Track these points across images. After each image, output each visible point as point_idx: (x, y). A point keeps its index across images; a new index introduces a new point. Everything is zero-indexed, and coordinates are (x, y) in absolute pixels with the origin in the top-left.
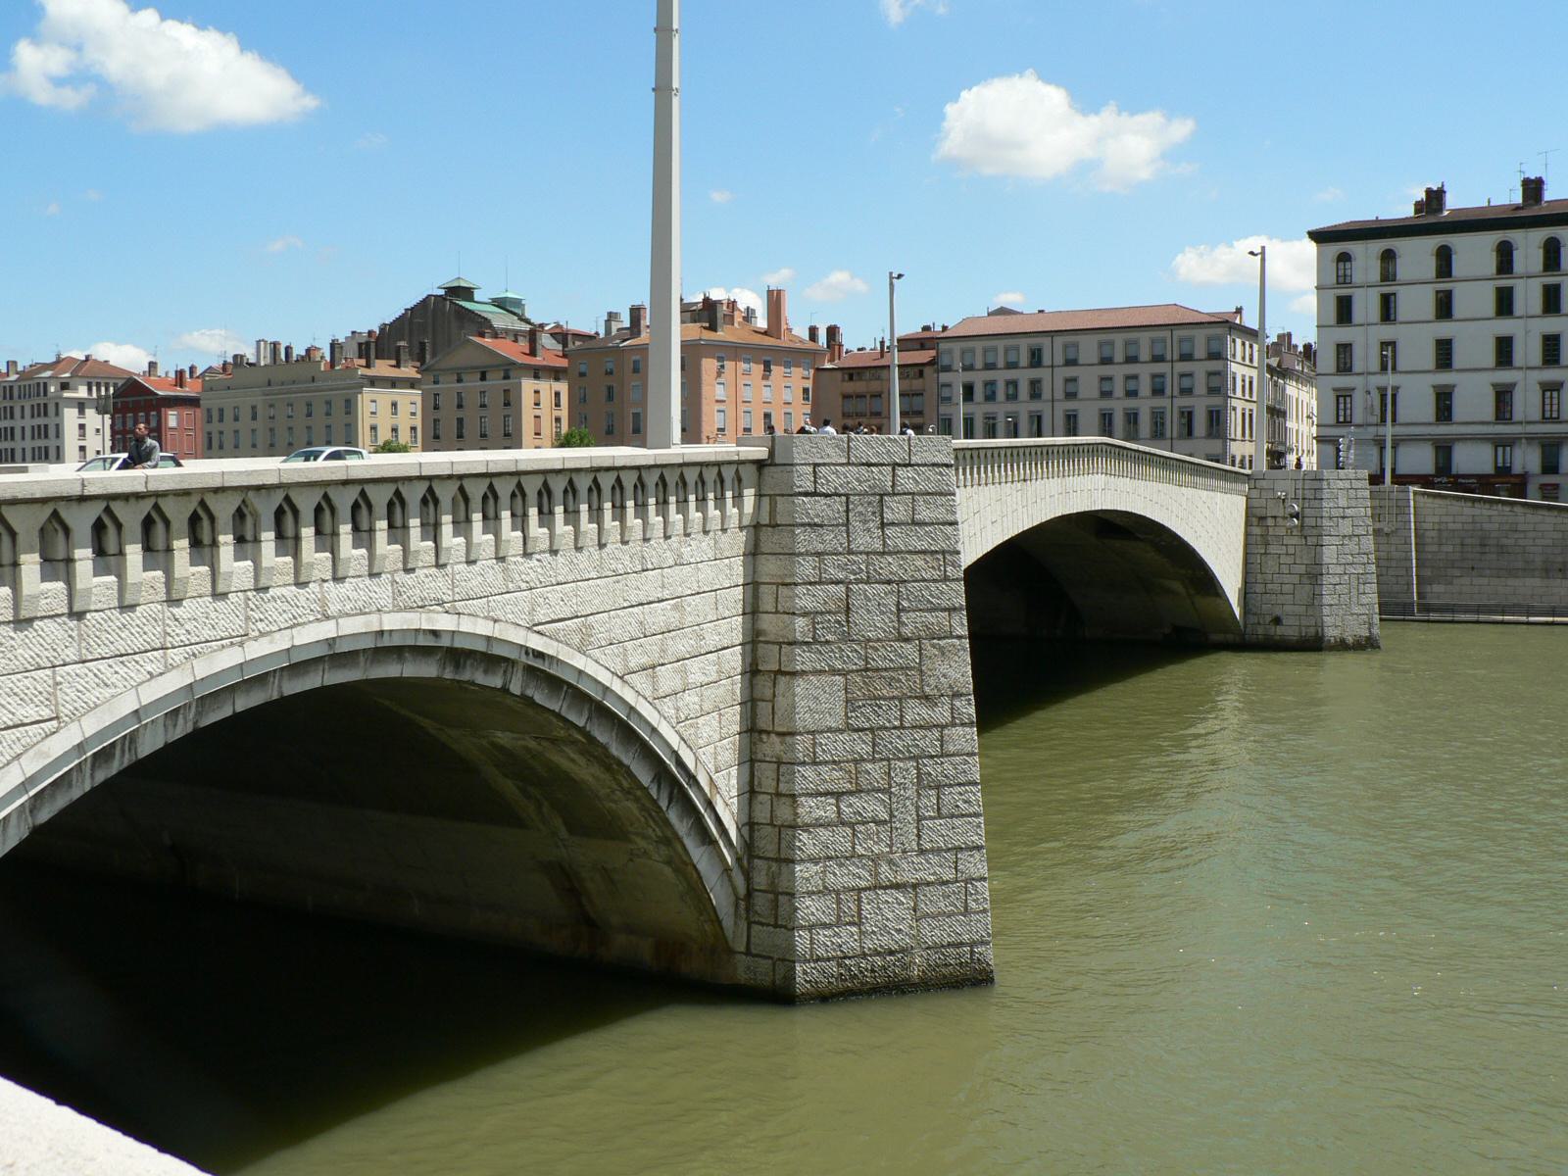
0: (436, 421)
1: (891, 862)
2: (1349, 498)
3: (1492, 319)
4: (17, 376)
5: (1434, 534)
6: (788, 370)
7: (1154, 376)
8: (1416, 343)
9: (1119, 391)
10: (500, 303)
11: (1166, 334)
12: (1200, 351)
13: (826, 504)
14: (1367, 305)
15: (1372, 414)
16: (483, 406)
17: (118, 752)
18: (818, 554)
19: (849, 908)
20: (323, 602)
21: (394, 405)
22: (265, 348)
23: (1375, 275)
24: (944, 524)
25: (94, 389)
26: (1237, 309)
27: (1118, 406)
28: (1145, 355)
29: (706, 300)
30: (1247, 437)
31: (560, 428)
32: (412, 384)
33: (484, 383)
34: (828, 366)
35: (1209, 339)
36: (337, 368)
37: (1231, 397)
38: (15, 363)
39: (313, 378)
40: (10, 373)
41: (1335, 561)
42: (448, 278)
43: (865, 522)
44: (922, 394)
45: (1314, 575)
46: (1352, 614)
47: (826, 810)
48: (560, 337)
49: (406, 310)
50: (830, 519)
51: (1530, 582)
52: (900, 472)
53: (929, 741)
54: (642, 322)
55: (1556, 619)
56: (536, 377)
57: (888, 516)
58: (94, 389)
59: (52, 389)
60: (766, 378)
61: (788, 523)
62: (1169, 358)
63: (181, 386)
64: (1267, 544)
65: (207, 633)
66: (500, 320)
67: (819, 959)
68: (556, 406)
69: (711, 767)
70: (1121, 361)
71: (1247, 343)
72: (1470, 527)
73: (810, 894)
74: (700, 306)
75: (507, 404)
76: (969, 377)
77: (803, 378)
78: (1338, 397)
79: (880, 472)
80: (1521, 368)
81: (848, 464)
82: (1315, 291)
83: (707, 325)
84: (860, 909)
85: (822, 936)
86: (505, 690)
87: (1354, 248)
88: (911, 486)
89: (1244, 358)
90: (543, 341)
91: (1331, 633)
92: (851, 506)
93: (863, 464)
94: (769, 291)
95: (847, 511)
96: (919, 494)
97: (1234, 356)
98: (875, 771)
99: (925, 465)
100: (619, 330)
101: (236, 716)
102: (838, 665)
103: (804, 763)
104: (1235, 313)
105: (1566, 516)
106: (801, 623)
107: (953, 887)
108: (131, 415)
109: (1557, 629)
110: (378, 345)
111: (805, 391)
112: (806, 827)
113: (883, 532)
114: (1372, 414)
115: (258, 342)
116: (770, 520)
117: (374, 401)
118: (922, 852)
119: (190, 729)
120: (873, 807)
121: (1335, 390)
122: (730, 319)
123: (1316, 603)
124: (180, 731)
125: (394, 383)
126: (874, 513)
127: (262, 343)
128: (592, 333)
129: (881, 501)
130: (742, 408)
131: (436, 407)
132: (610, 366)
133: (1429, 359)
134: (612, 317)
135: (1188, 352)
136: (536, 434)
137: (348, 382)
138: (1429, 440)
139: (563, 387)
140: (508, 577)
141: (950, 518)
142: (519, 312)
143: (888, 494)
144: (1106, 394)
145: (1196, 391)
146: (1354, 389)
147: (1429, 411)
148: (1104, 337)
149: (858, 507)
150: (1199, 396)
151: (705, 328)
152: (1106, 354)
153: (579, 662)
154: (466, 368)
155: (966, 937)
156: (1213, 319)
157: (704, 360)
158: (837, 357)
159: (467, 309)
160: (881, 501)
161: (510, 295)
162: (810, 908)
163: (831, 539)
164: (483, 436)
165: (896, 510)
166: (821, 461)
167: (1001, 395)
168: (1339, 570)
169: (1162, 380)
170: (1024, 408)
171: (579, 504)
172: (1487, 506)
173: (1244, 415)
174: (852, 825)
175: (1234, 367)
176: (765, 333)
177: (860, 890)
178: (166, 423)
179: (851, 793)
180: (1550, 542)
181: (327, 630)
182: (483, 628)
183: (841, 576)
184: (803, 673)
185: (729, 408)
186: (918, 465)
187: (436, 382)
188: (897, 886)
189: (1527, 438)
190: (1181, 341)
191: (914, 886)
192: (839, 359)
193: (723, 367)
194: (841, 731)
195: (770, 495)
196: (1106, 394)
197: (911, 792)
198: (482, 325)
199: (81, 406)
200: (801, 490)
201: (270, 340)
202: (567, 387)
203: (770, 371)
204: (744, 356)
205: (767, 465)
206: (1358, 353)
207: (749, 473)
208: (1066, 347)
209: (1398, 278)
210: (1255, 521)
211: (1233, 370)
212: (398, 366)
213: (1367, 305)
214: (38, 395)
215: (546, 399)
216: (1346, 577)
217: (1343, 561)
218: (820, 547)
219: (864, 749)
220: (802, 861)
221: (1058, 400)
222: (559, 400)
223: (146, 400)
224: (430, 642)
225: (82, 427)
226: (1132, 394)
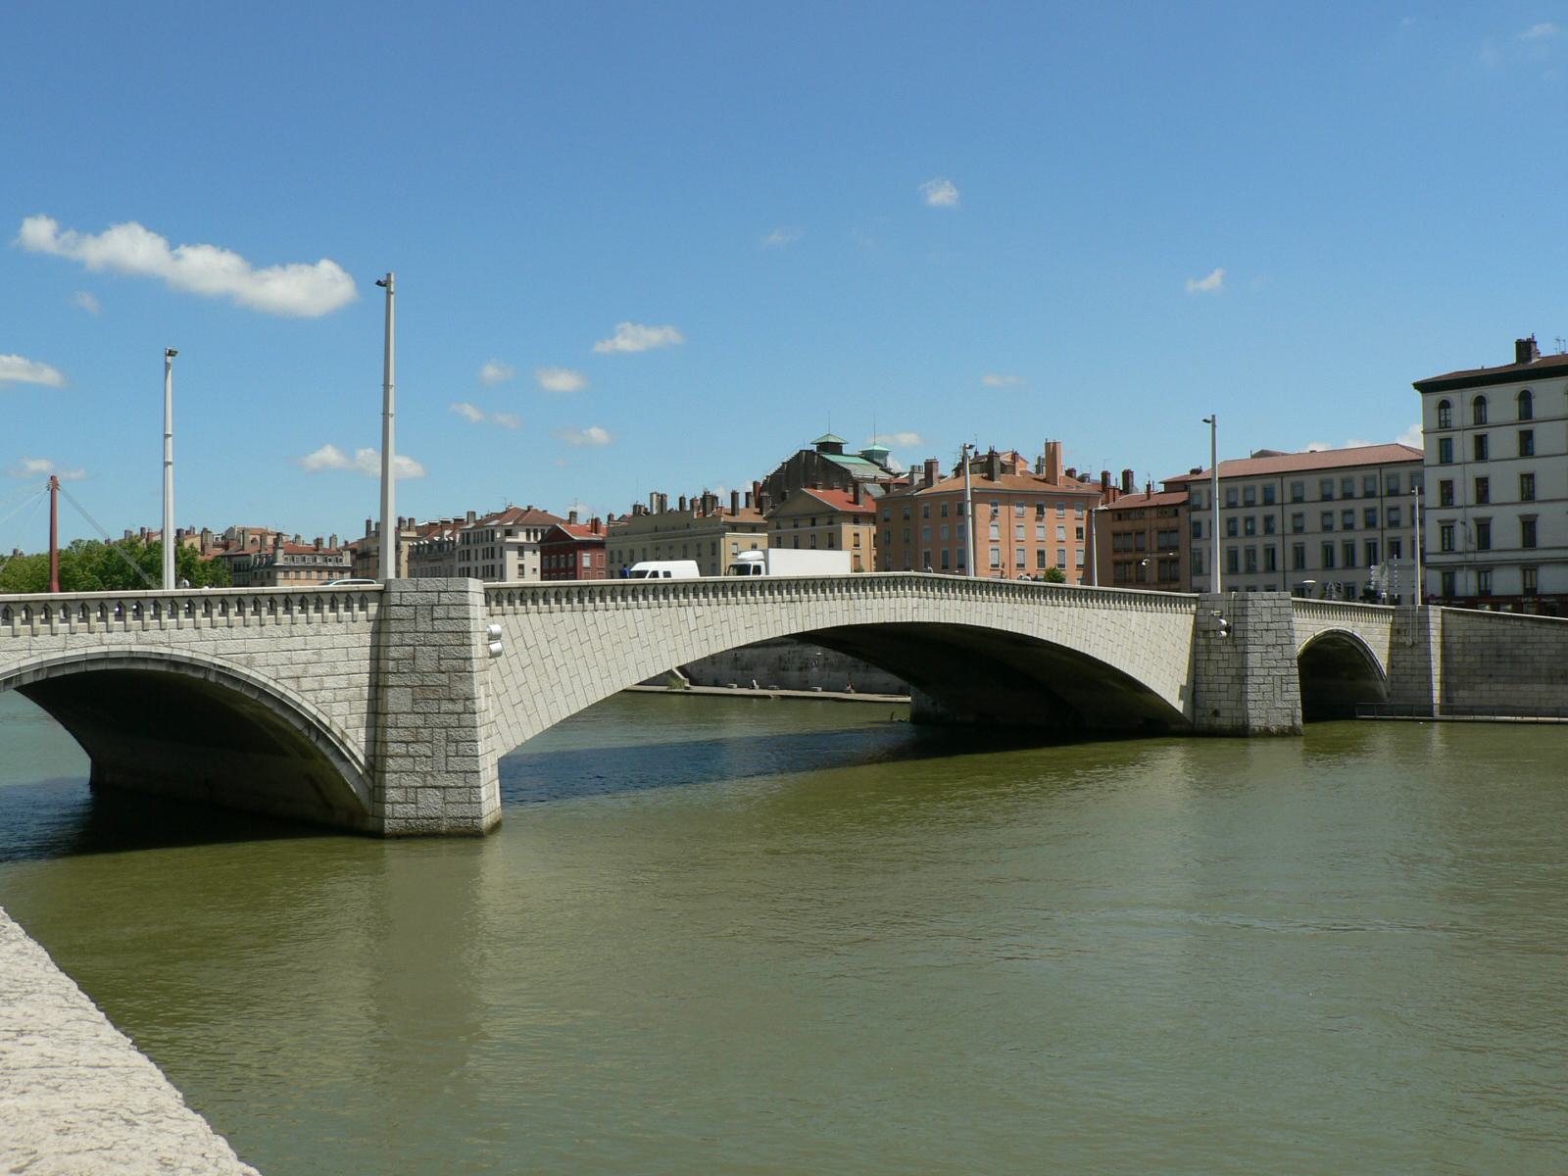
1: (433, 776)
2: (1272, 615)
3: (1517, 459)
5: (1459, 646)
7: (1367, 511)
8: (1505, 482)
9: (1338, 525)
10: (868, 456)
11: (1376, 472)
14: (1463, 446)
15: (1470, 542)
17: (14, 681)
18: (401, 632)
19: (411, 794)
20: (101, 639)
23: (1470, 420)
25: (532, 534)
28: (1358, 491)
33: (815, 528)
38: (474, 513)
39: (688, 525)
41: (1258, 666)
42: (820, 435)
44: (1176, 531)
45: (1241, 677)
46: (1276, 708)
47: (402, 749)
49: (783, 463)
51: (1537, 687)
52: (442, 595)
53: (453, 720)
55: (1540, 719)
56: (856, 522)
57: (435, 615)
58: (532, 534)
59: (498, 535)
60: (1038, 519)
62: (1379, 494)
63: (596, 533)
64: (1209, 652)
65: (48, 646)
67: (396, 818)
69: (343, 726)
72: (1486, 639)
73: (393, 787)
78: (1443, 528)
80: (1461, 507)
82: (1422, 435)
84: (416, 796)
85: (398, 807)
86: (205, 679)
87: (1452, 396)
88: (447, 601)
91: (1256, 723)
95: (416, 613)
98: (426, 733)
101: (65, 676)
102: (409, 683)
103: (391, 727)
105: (1566, 628)
106: (391, 663)
107: (464, 790)
109: (1561, 727)
111: (1079, 530)
112: (391, 757)
114: (1470, 542)
115: (652, 494)
118: (448, 772)
119: (45, 677)
120: (423, 749)
121: (1439, 521)
123: (1243, 699)
124: (40, 677)
127: (655, 496)
132: (907, 512)
133: (1515, 494)
135: (1299, 495)
137: (713, 528)
138: (1516, 564)
140: (201, 635)
141: (466, 616)
142: (881, 462)
144: (1327, 528)
145: (1357, 527)
146: (1454, 521)
147: (1515, 538)
148: (1345, 475)
151: (984, 478)
153: (246, 671)
155: (469, 815)
161: (876, 448)
162: (392, 794)
163: (408, 626)
165: (439, 612)
167: (1241, 531)
168: (1263, 672)
172: (1558, 627)
174: (413, 757)
177: (417, 788)
178: (581, 562)
179: (413, 742)
180: (1553, 652)
181: (104, 649)
182: (188, 654)
183: (412, 643)
184: (392, 686)
185: (1003, 548)
188: (435, 787)
189: (1467, 566)
190: (1388, 478)
191: (444, 788)
193: (996, 511)
194: (410, 714)
196: (1327, 528)
197: (443, 743)
199: (521, 549)
201: (661, 493)
203: (1043, 514)
206: (1457, 489)
207: (1143, 597)
208: (1293, 486)
209: (1488, 420)
210: (1201, 634)
213: (1463, 446)
214: (487, 540)
216: (1270, 678)
217: (1267, 665)
218: (402, 629)
219: (420, 722)
220: (389, 772)
221: (1288, 534)
224: (158, 657)
225: (521, 567)
226: (1348, 527)
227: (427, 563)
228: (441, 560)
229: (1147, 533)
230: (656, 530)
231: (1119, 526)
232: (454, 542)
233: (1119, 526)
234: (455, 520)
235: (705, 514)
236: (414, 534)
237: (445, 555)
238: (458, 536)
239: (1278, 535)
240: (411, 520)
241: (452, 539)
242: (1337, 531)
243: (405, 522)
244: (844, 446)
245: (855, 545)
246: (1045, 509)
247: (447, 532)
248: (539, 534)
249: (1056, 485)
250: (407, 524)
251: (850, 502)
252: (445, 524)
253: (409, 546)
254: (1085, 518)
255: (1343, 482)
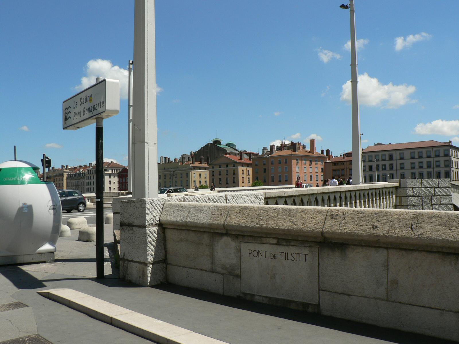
0: (213, 179)
4: (92, 167)
6: (317, 163)
7: (428, 162)
9: (417, 166)
10: (228, 145)
11: (431, 149)
12: (442, 154)
13: (416, 199)
16: (227, 175)
21: (200, 175)
22: (163, 159)
24: (449, 204)
26: (450, 141)
27: (417, 171)
28: (424, 156)
29: (292, 143)
30: (457, 180)
31: (249, 181)
32: (205, 168)
33: (227, 168)
34: (328, 161)
35: (444, 150)
36: (184, 164)
37: (452, 168)
39: (177, 167)
40: (90, 167)
42: (214, 138)
43: (427, 204)
48: (248, 154)
49: (202, 147)
50: (417, 203)
52: (436, 189)
54: (274, 150)
56: (243, 166)
57: (434, 202)
61: (406, 205)
62: (432, 156)
66: (229, 150)
68: (248, 174)
70: (417, 157)
71: (456, 151)
74: (290, 145)
75: (234, 174)
76: (370, 164)
77: (321, 165)
79: (431, 189)
81: (422, 187)
83: (293, 150)
88: (439, 194)
89: (455, 156)
90: (244, 156)
92: (423, 200)
93: (426, 187)
94: (310, 140)
95: (422, 201)
96: (442, 196)
97: (452, 155)
99: (442, 187)
100: (266, 152)
104: (449, 142)
108: (124, 178)
110: (196, 156)
111: (322, 169)
113: (432, 207)
115: (161, 157)
116: (400, 204)
117: (195, 174)
122: (299, 148)
125: (200, 168)
126: (429, 201)
127: (162, 157)
128: (257, 153)
129: (431, 198)
130: (304, 174)
131: (213, 175)
132: (265, 162)
134: (264, 148)
135: (403, 157)
136: (243, 183)
139: (250, 169)
142: (234, 148)
143: (433, 196)
144: (413, 168)
148: (383, 153)
149: (425, 200)
150: (417, 169)
151: (292, 151)
152: (413, 156)
154: (229, 163)
156: (445, 145)
157: (292, 160)
158: (330, 159)
159: (219, 147)
160: (431, 198)
161: (231, 143)
164: (227, 183)
165: (436, 200)
166: (414, 187)
167: (381, 169)
169: (430, 163)
170: (388, 173)
171: (365, 199)
173: (456, 173)
175: (452, 159)
176: (309, 152)
186: (441, 187)
187: (213, 168)
192: (331, 159)
193: (298, 162)
195: (399, 197)
196: (413, 168)
198: (224, 151)
199: (110, 175)
200: (409, 195)
202: (252, 169)
203: (311, 163)
204: (304, 159)
205: (398, 188)
207: (394, 190)
208: (400, 154)
211: (452, 159)
212: (201, 163)
215: (245, 172)
221: (398, 170)
222: (249, 172)
223: (125, 174)
225: (110, 181)
226: (421, 167)
227: (74, 180)
228: (80, 179)
229: (345, 170)
230: (164, 169)
231: (335, 167)
232: (85, 173)
233: (335, 167)
234: (84, 166)
235: (182, 164)
236: (68, 171)
237: (81, 177)
238: (86, 171)
239: (394, 170)
240: (67, 166)
241: (84, 172)
242: (417, 169)
243: (64, 166)
244: (221, 142)
245: (242, 174)
246: (312, 162)
247: (81, 170)
248: (118, 171)
249: (314, 154)
250: (65, 168)
251: (239, 159)
252: (80, 167)
253: (67, 174)
254: (323, 164)
255: (419, 153)
